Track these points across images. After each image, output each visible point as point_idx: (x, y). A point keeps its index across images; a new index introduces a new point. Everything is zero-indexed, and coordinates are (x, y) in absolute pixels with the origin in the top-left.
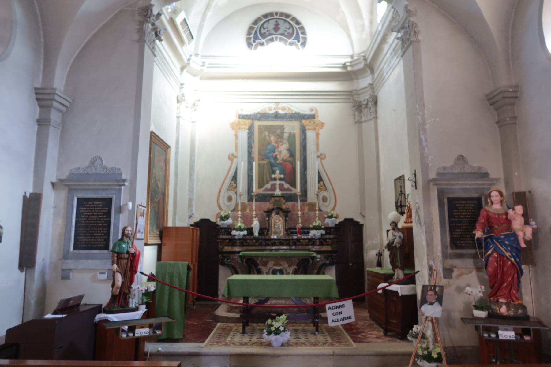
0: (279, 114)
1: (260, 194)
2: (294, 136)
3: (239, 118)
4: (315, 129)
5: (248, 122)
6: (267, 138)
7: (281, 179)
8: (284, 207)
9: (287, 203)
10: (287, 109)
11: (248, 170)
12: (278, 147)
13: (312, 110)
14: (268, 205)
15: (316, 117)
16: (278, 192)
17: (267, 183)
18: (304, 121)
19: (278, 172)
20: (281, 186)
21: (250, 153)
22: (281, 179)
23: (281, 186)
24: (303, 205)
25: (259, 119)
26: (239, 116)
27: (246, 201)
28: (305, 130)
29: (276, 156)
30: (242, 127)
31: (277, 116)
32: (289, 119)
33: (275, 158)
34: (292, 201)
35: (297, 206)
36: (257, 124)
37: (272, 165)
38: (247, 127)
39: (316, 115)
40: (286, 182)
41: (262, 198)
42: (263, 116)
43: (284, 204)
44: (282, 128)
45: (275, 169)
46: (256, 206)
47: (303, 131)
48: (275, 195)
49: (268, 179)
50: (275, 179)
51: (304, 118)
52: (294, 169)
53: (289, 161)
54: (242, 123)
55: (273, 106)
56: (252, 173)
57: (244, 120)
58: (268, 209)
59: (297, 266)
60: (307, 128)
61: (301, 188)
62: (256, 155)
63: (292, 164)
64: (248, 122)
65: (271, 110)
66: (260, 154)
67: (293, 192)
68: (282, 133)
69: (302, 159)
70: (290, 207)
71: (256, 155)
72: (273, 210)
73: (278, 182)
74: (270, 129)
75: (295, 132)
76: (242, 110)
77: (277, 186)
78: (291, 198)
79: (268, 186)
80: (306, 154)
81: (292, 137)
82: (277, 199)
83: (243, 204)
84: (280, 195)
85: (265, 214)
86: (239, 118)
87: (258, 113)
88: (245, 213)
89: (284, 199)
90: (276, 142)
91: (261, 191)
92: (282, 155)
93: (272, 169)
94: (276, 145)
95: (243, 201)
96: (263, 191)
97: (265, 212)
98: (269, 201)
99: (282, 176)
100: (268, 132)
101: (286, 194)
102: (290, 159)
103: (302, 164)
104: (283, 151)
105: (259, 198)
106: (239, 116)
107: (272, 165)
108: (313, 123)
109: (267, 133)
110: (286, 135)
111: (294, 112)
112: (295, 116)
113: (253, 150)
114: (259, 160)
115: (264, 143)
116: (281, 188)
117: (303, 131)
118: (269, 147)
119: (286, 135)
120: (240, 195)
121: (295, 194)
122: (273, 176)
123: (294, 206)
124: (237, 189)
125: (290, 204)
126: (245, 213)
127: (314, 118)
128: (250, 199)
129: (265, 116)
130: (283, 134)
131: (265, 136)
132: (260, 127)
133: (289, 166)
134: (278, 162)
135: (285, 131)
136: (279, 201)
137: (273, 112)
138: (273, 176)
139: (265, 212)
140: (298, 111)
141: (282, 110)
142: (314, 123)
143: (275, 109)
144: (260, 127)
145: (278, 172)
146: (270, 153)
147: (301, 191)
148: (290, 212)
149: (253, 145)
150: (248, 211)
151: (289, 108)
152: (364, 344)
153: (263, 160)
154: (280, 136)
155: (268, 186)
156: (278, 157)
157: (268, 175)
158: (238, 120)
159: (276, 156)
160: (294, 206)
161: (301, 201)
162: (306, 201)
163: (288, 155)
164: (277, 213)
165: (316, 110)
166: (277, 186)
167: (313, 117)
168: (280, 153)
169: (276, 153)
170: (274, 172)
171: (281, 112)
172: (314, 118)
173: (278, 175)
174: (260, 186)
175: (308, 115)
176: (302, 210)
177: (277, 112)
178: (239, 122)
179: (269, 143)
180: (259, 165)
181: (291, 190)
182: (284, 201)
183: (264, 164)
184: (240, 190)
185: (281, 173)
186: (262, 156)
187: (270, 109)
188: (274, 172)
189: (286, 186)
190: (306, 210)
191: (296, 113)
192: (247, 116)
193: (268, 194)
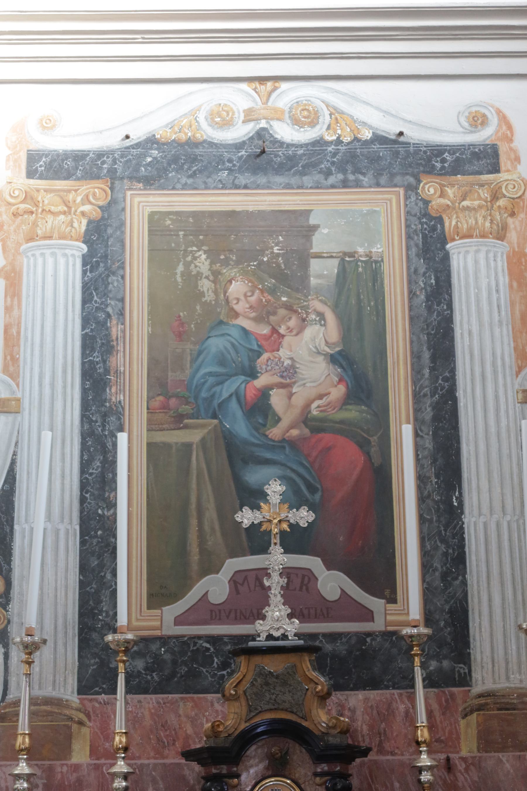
0: (276, 142)
1: (164, 640)
2: (374, 268)
3: (31, 174)
4: (501, 234)
5: (87, 198)
6: (206, 285)
7: (296, 540)
8: (321, 718)
9: (337, 697)
10: (326, 119)
11: (83, 486)
12: (276, 338)
13: (478, 120)
14: (215, 714)
15: (504, 162)
16: (277, 621)
17: (210, 567)
18: (429, 188)
19: (275, 489)
20: (298, 584)
21: (95, 381)
22: (296, 540)
23: (298, 584)
24: (447, 707)
25: (154, 179)
26: (33, 157)
27: (68, 691)
28: (443, 240)
29: (264, 394)
30: (50, 223)
31: (262, 158)
32: (337, 177)
33: (259, 409)
34: (374, 684)
35: (410, 718)
36: (141, 205)
37: (236, 455)
38: (82, 226)
39: (503, 149)
40: (329, 565)
41: (173, 667)
42: (176, 160)
43: (323, 698)
44: (299, 226)
45: (253, 476)
46: (132, 720)
47: (430, 244)
48: (261, 642)
49: (216, 541)
50: (256, 540)
51: (430, 171)
52: (380, 479)
53: (344, 429)
54: (47, 200)
55: (240, 99)
56: (113, 505)
57: (60, 184)
58: (214, 732)
59: (46, 780)
60: (450, 223)
61: (428, 593)
62: (133, 390)
63: (363, 444)
64: (87, 198)
65: (227, 124)
66: (158, 384)
67: (378, 625)
68: (303, 258)
69: (428, 414)
70: (362, 725)
71: (133, 390)
72: (246, 739)
73: (277, 558)
74: (220, 234)
75: (377, 249)
76: (47, 125)
77: (275, 583)
78: (366, 662)
79: (216, 587)
80: (452, 380)
81: (358, 280)
82: (274, 665)
83: (46, 708)
84: (293, 641)
85: (194, 770)
86: (31, 174)
87: (151, 141)
88: (61, 768)
89: (320, 667)
90: (263, 313)
91: (167, 621)
92: (301, 394)
93: (237, 479)
94: (265, 330)
95: (48, 692)
96: (179, 621)
97: (189, 755)
98: (218, 688)
99: (304, 516)
100: (213, 255)
101: (333, 637)
102: (352, 413)
103: (428, 443)
104: (306, 365)
105: (156, 664)
106: (33, 157)
107: (236, 455)
108: (485, 194)
109: (203, 263)
110: (322, 272)
111: (367, 135)
112: (374, 159)
113: (117, 361)
114: (153, 426)
115: (183, 321)
116: (300, 590)
117: (430, 244)
118: (216, 344)
119: (322, 272)
120: (31, 649)
121: (391, 636)
122: (246, 517)
123: (385, 714)
124: (14, 606)
125: (357, 704)
126: (61, 768)
127: (495, 169)
128: (96, 678)
129: (193, 159)
130: (305, 265)
131: (192, 279)
132: (155, 221)
133: (348, 459)
134: (275, 433)
135: (319, 243)
136: (284, 680)
137: (240, 132)
138: (246, 517)
139: (189, 755)
140: (391, 128)
141: (296, 122)
142: (495, 196)
143: (249, 116)
144: (155, 221)
145: (275, 489)
146: (221, 379)
147: (429, 619)
148: (365, 752)
149: (115, 331)
150: (80, 755)
151: (336, 113)
152: (3, 315)
153: (179, 421)
154: (286, 277)
155: (216, 587)
156: (277, 400)
157: (211, 513)
158: (22, 182)
159: (264, 394)
160: (385, 714)
161: (430, 682)
162: (465, 681)
163: (338, 392)
164: (278, 766)
165: (503, 119)
166: (275, 583)
167: (486, 159)
168: (289, 375)
169: (261, 382)
170: (254, 497)
171: (285, 132)
172: (495, 169)
173: (276, 507)
174: (160, 594)
175: (453, 149)
176: (442, 741)
177: (261, 134)
178: (28, 197)
179: (218, 318)
180: (155, 452)
181: (367, 615)
182: (323, 681)
183: (188, 447)
184: (31, 619)
185: (295, 499)
186: (172, 402)
187: (222, 118)
188: (254, 497)
189: (332, 583)
190: (468, 747)
191: (379, 139)
192: (79, 157)
193: (214, 640)
